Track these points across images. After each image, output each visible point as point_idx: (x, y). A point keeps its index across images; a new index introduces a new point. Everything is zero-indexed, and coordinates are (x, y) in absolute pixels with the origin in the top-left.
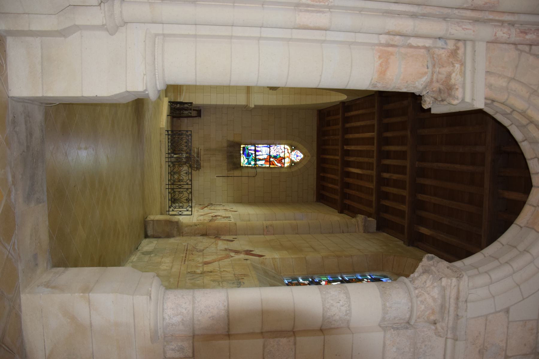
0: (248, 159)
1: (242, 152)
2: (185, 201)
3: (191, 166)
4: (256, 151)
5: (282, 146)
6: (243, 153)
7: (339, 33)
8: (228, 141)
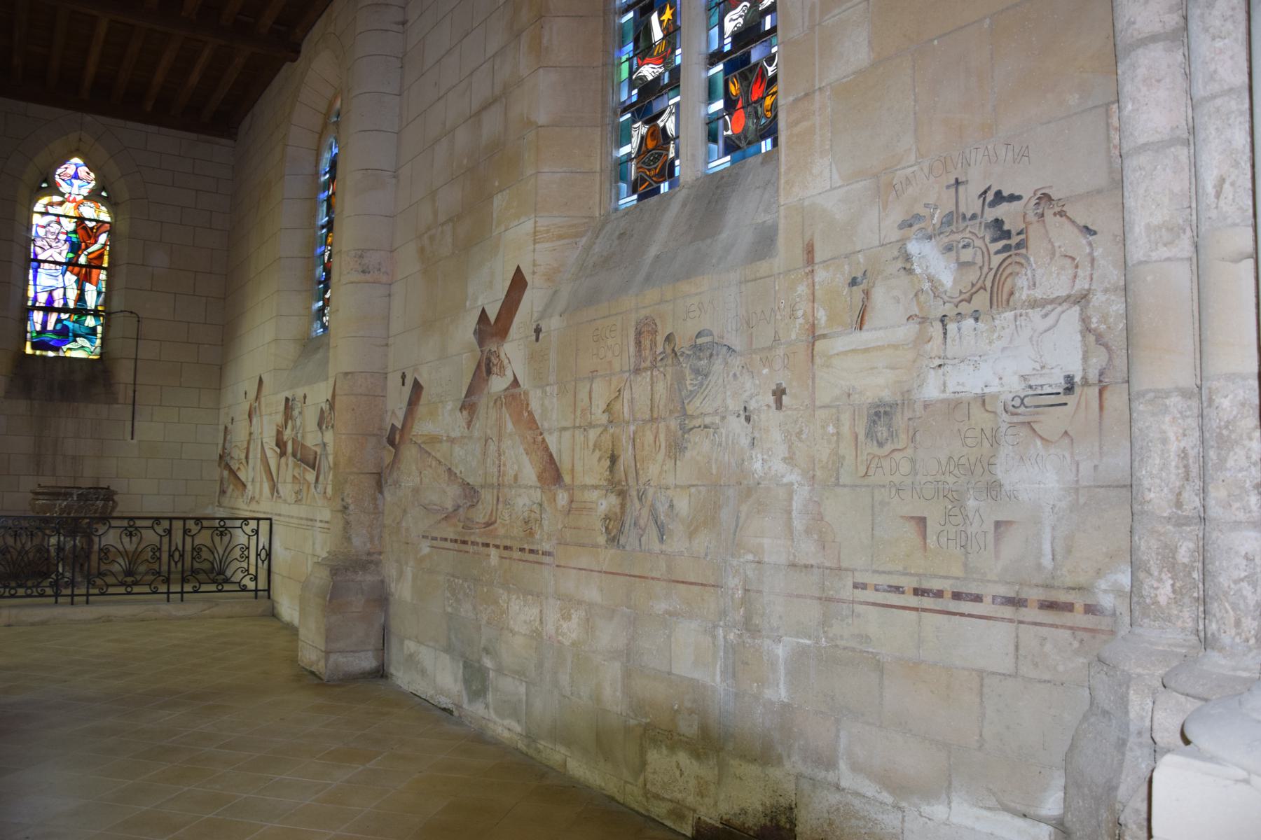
0: (76, 336)
1: (51, 354)
2: (226, 539)
3: (105, 519)
4: (49, 308)
5: (37, 219)
6: (56, 349)
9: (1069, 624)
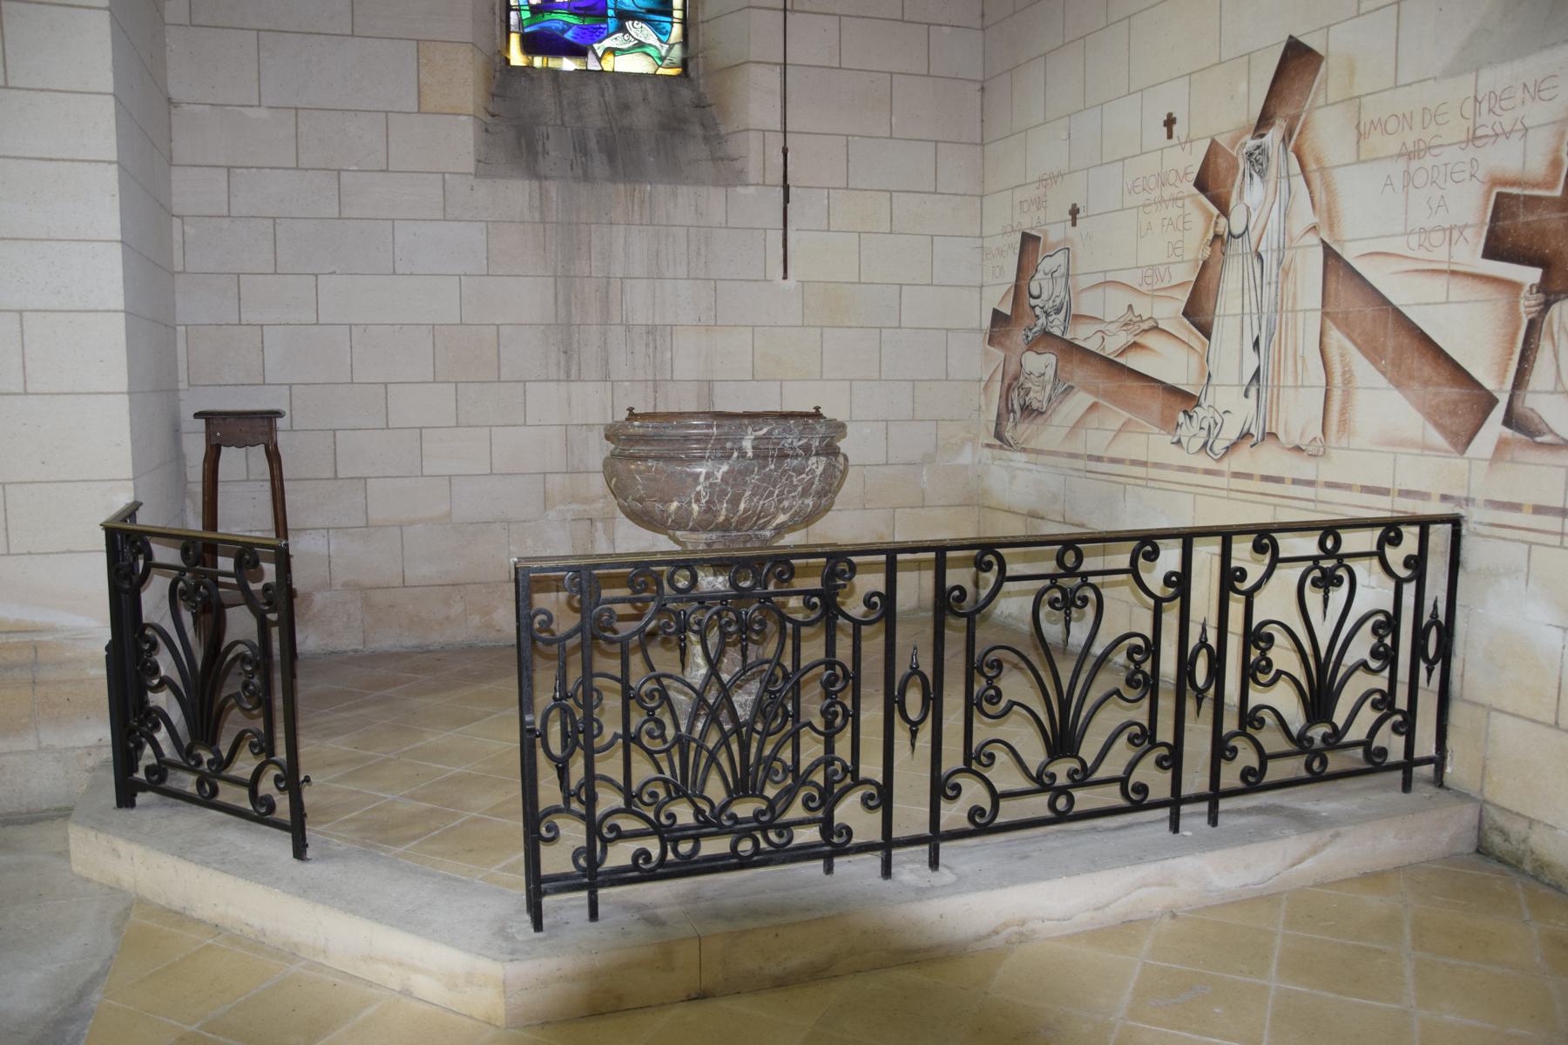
2: (1339, 595)
6: (578, 51)
7: (1528, 723)
8: (485, 167)
9: (1234, 435)
